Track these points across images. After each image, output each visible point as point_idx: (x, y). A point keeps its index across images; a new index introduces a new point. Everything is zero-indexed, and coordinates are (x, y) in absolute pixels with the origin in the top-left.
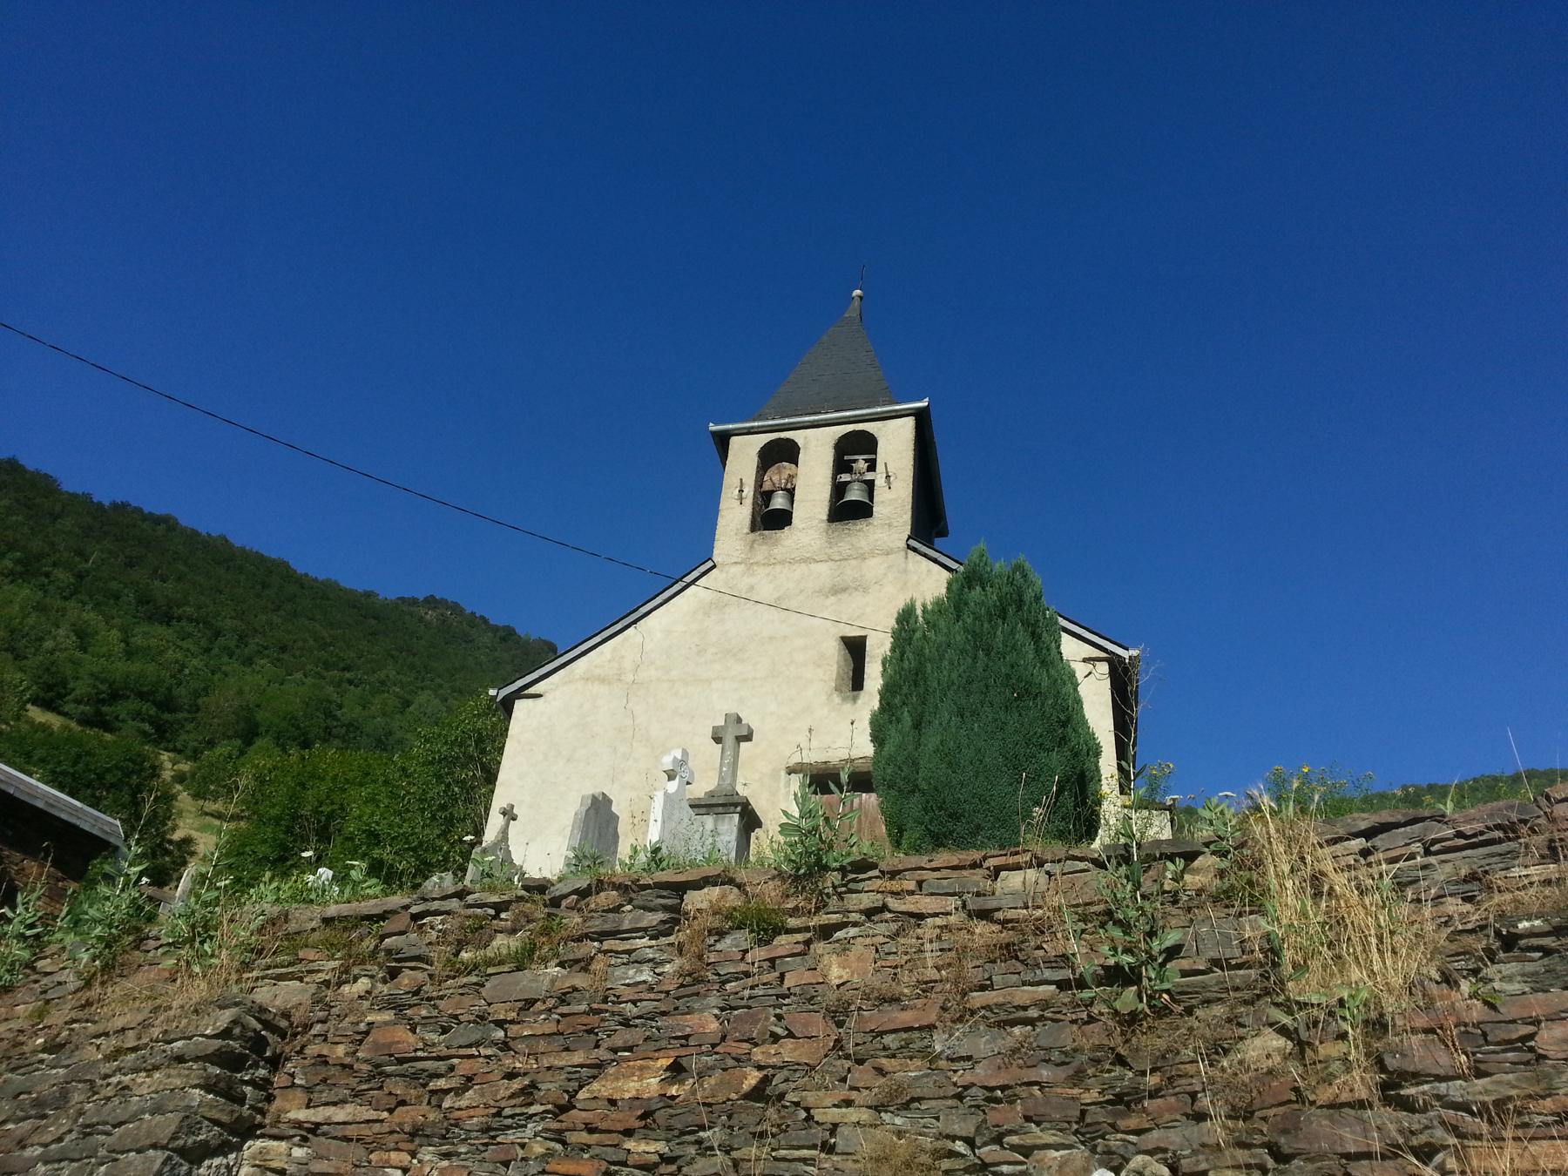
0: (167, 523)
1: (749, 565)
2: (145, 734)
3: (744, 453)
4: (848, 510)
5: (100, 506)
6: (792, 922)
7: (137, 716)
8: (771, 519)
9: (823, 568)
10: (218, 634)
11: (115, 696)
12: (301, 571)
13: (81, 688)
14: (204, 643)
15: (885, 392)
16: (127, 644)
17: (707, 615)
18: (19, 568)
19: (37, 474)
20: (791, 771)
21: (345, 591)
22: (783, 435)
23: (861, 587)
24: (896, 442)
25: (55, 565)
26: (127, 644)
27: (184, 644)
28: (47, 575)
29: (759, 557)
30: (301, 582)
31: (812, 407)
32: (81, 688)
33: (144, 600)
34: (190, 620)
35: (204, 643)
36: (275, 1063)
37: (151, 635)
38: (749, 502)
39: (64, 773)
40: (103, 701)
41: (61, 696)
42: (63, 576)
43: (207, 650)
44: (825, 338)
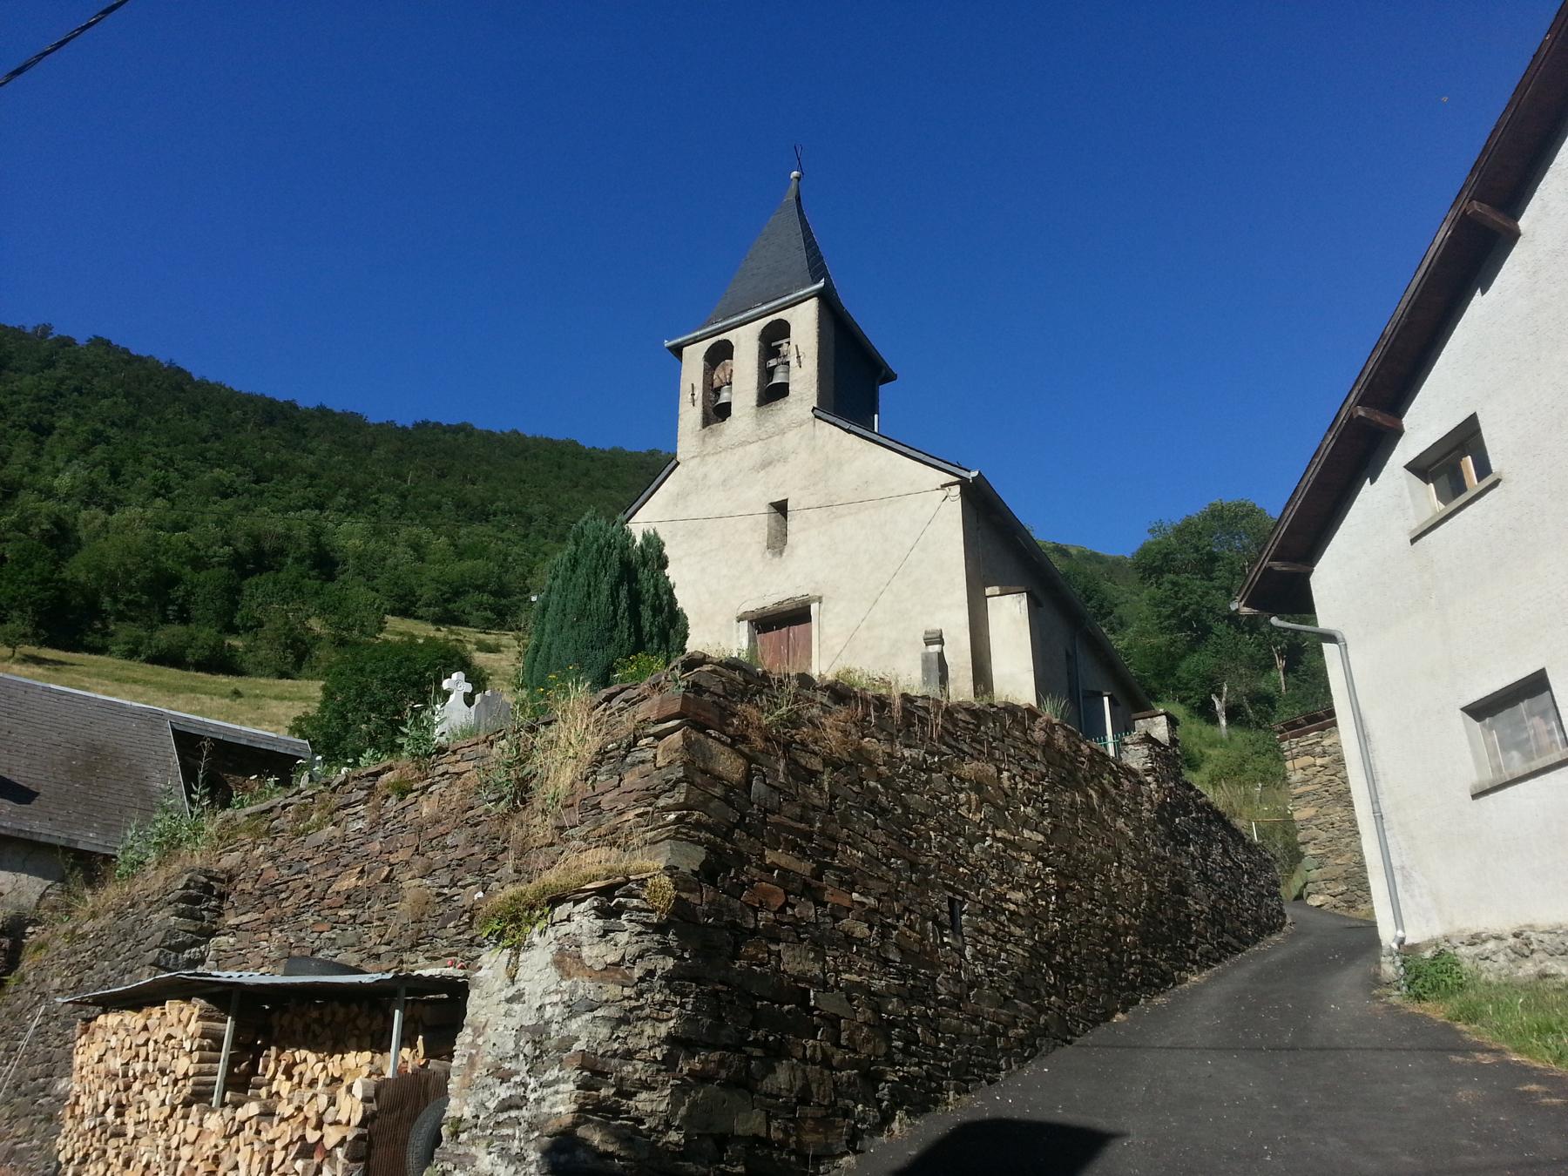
0: (464, 429)
1: (702, 456)
2: (487, 620)
3: (695, 357)
4: (772, 393)
5: (404, 428)
6: (415, 786)
7: (480, 606)
8: (717, 412)
9: (754, 448)
10: (530, 519)
11: (457, 594)
12: (588, 446)
13: (427, 593)
14: (521, 531)
15: (780, 292)
16: (456, 546)
17: (676, 505)
18: (351, 501)
19: (344, 414)
20: (740, 620)
21: (631, 455)
22: (720, 337)
23: (782, 459)
24: (804, 320)
25: (379, 491)
26: (456, 546)
27: (505, 535)
28: (375, 502)
29: (709, 449)
30: (591, 456)
31: (737, 312)
32: (427, 593)
33: (461, 504)
34: (504, 512)
35: (521, 531)
36: (222, 897)
37: (469, 533)
38: (699, 403)
39: (393, 679)
40: (448, 601)
41: (414, 604)
42: (389, 499)
43: (526, 536)
44: (766, 229)
